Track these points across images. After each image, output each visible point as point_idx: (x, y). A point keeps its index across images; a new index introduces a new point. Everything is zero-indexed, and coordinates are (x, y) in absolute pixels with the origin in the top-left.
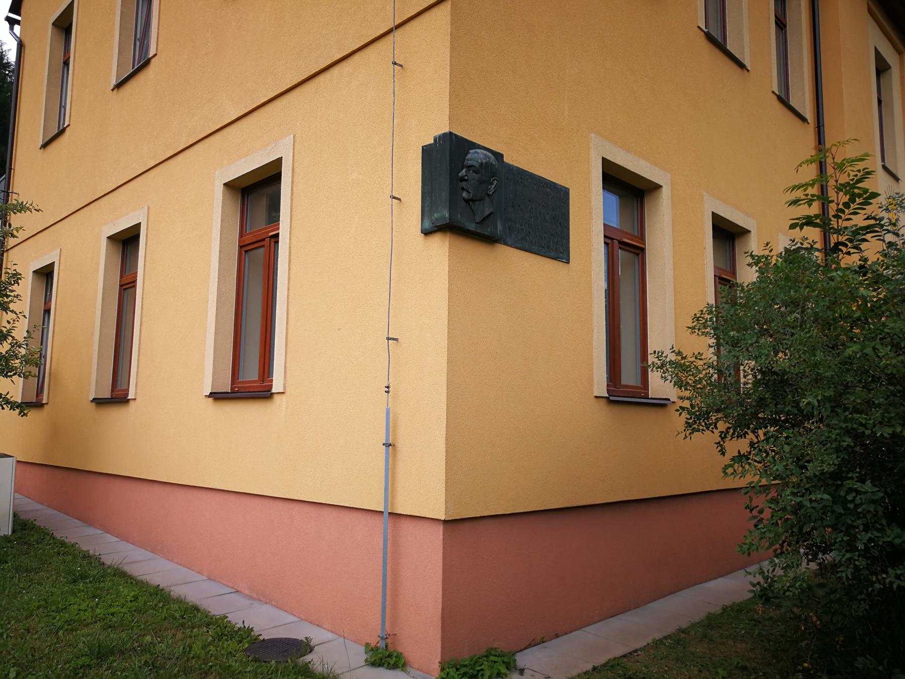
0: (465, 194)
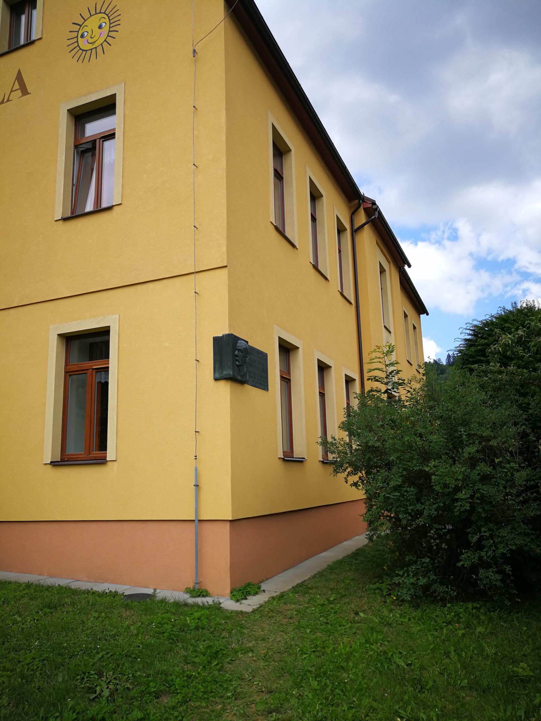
0: (237, 363)
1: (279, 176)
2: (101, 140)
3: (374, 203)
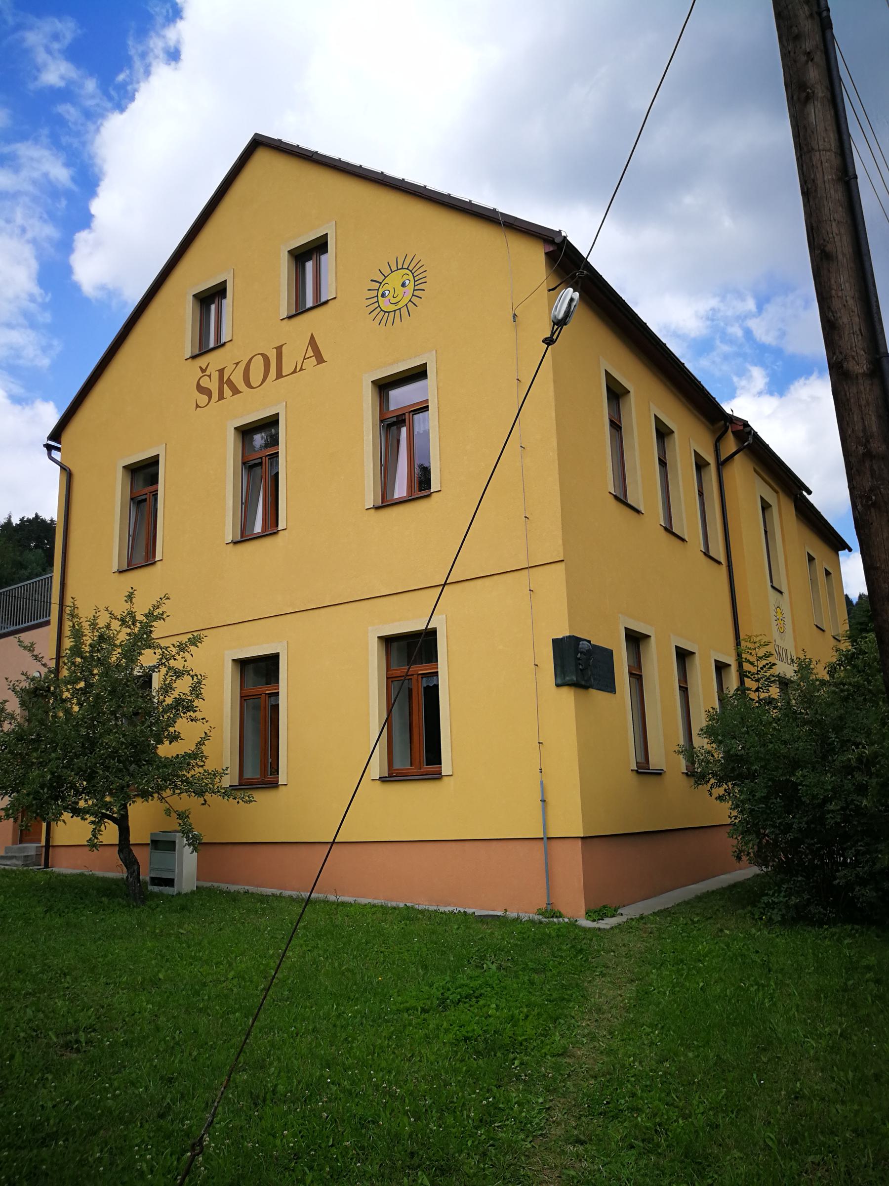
1: (616, 426)
2: (411, 414)
3: (746, 424)
